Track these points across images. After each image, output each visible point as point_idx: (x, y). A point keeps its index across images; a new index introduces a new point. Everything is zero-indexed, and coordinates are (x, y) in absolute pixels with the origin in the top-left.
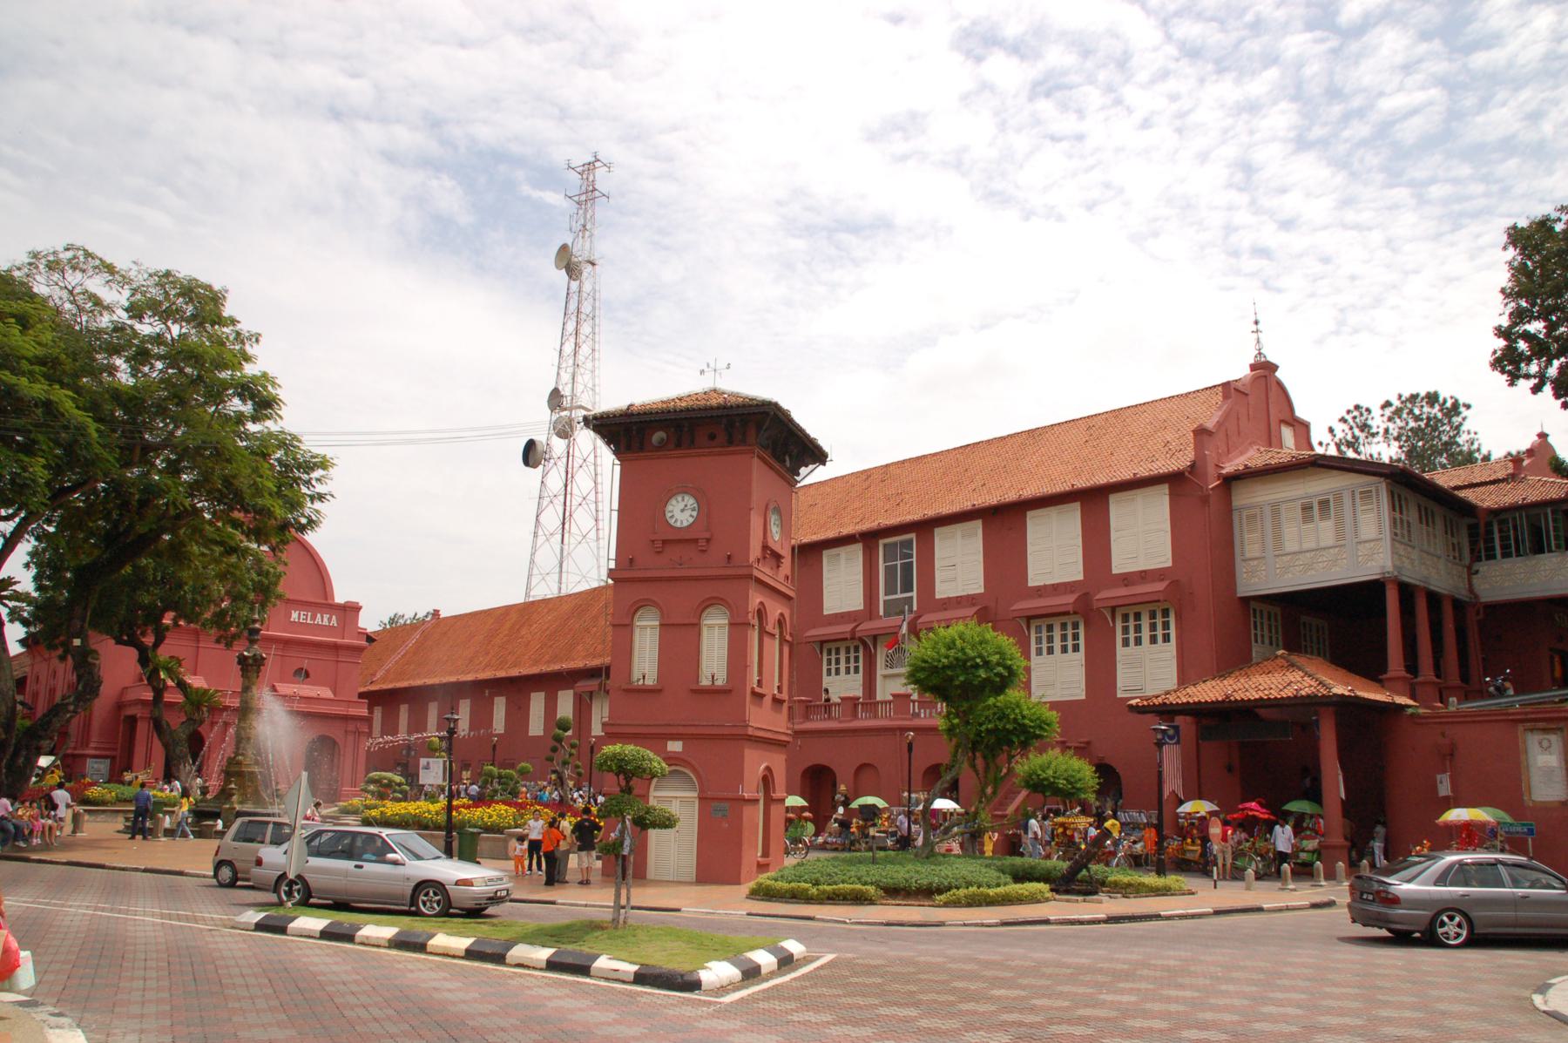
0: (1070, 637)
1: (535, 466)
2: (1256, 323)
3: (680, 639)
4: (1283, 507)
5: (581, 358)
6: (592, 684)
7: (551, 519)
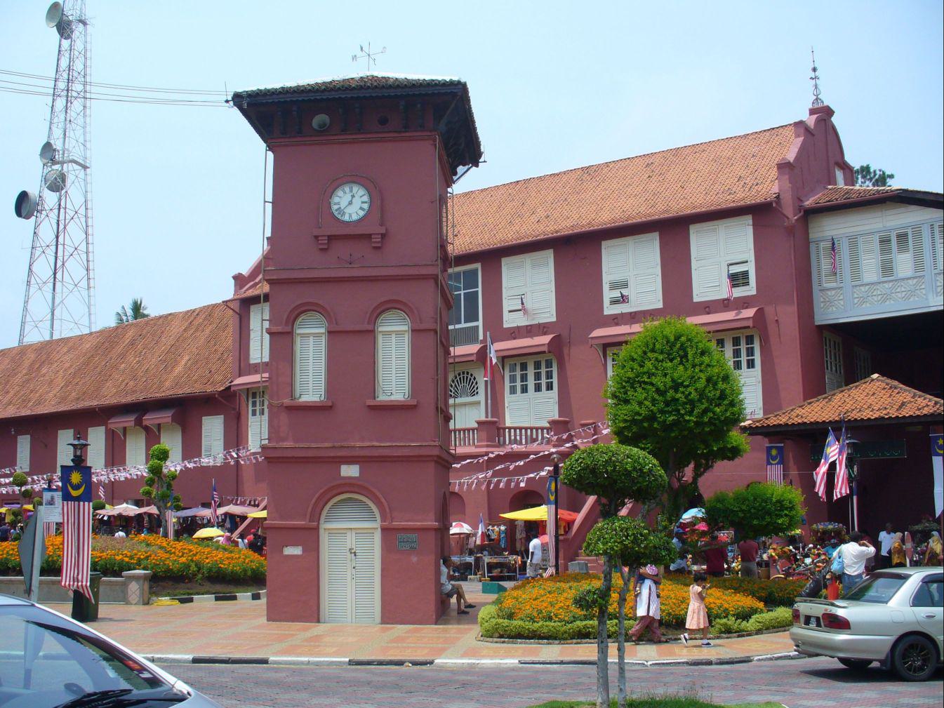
0: (744, 352)
1: (27, 217)
2: (814, 70)
3: (350, 348)
4: (861, 240)
5: (72, 114)
6: (129, 421)
7: (43, 269)
